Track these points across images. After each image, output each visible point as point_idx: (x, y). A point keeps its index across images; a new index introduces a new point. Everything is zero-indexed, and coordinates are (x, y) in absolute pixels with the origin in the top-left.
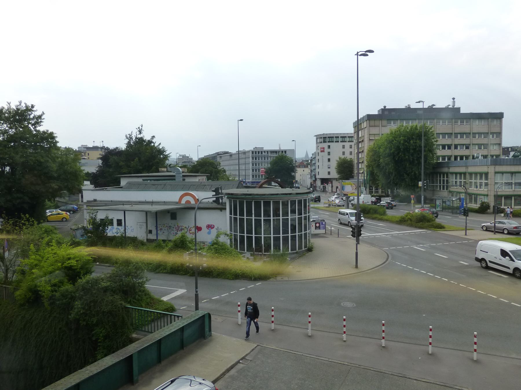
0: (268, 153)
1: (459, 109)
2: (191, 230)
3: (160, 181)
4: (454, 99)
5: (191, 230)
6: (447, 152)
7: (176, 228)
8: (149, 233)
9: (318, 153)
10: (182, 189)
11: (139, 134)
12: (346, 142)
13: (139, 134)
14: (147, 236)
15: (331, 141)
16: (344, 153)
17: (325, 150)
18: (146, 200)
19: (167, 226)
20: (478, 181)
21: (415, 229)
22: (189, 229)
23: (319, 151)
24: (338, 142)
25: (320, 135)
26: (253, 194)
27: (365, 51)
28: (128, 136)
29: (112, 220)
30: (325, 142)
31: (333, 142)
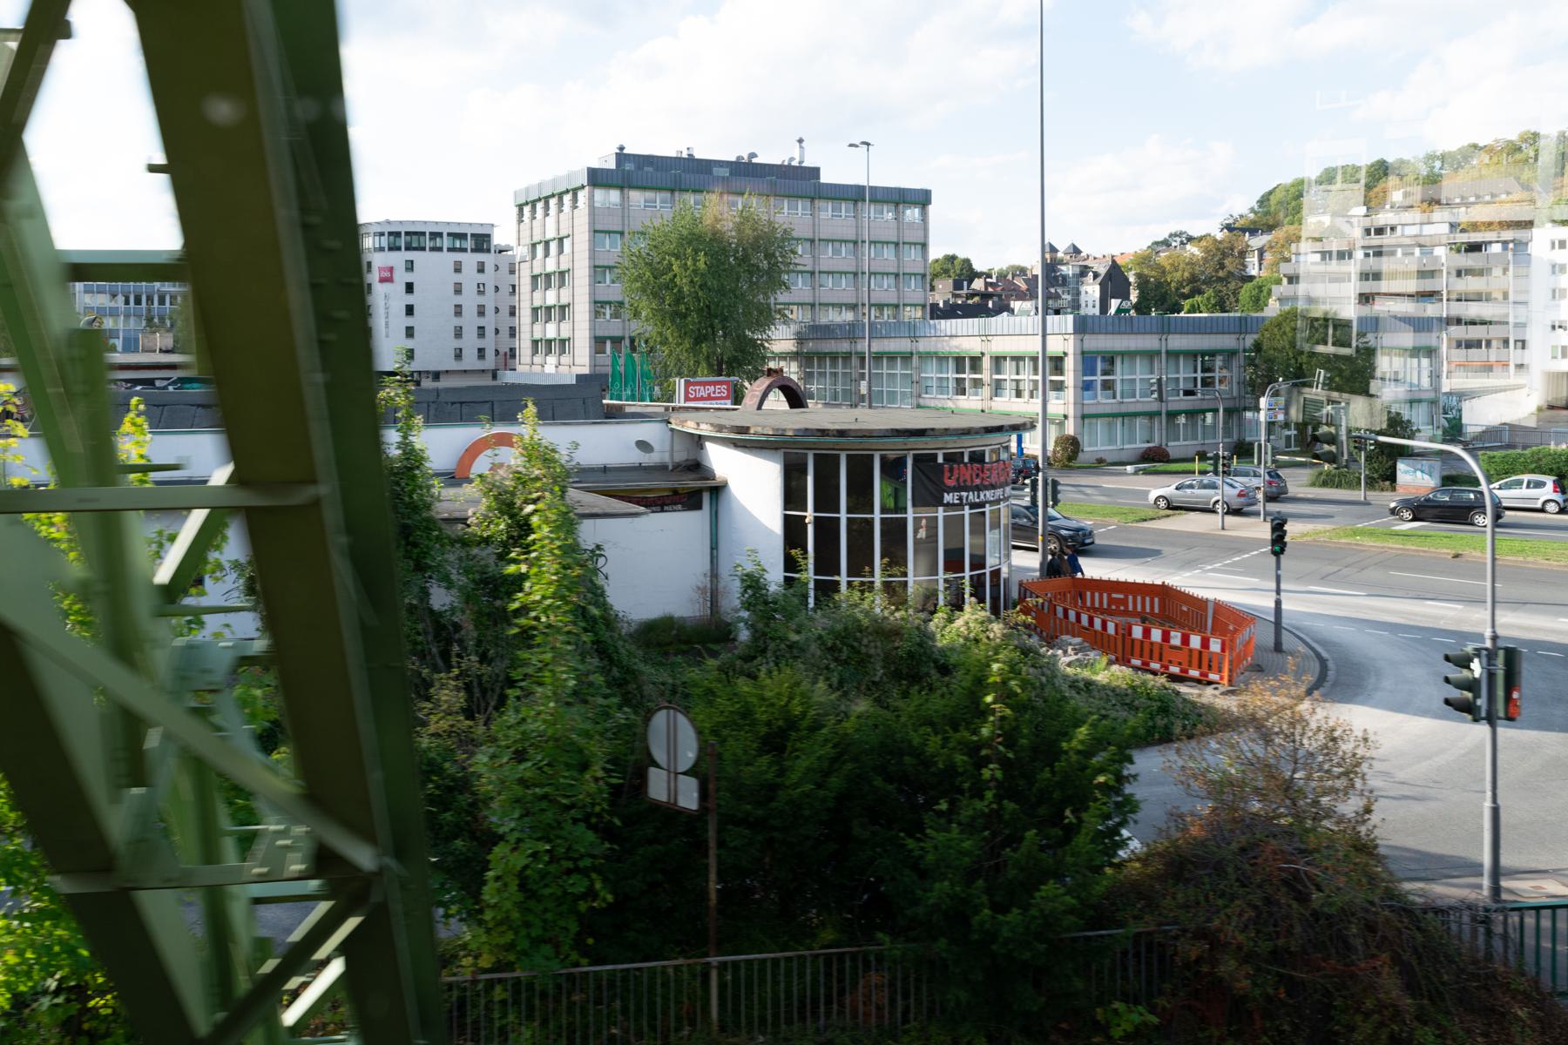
1: (815, 172)
4: (801, 141)
17: (396, 276)
24: (440, 249)
26: (933, 429)
30: (394, 248)
31: (423, 249)
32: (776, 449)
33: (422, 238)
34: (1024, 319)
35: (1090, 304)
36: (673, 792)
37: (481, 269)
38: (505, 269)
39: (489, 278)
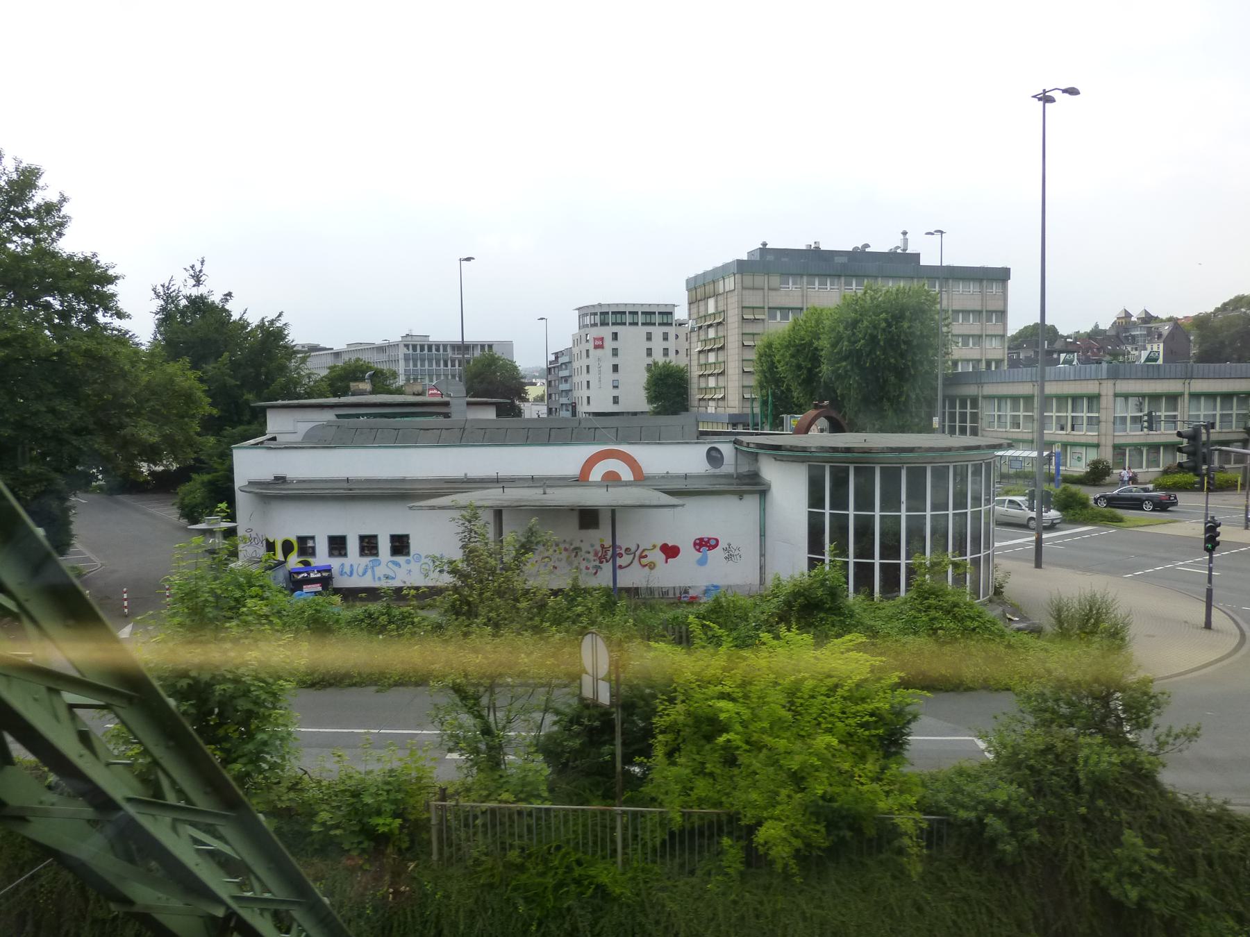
0: (445, 350)
1: (918, 255)
2: (646, 556)
3: (395, 417)
4: (905, 233)
5: (646, 556)
6: (972, 352)
7: (596, 554)
9: (588, 351)
10: (593, 440)
11: (194, 286)
12: (654, 324)
13: (194, 286)
15: (619, 321)
16: (649, 352)
18: (466, 475)
19: (566, 550)
21: (1070, 526)
22: (638, 554)
23: (591, 346)
24: (637, 324)
25: (593, 306)
26: (920, 448)
27: (1063, 88)
28: (160, 290)
30: (604, 324)
31: (625, 324)
32: (803, 462)
33: (653, 316)
36: (596, 692)
39: (671, 344)
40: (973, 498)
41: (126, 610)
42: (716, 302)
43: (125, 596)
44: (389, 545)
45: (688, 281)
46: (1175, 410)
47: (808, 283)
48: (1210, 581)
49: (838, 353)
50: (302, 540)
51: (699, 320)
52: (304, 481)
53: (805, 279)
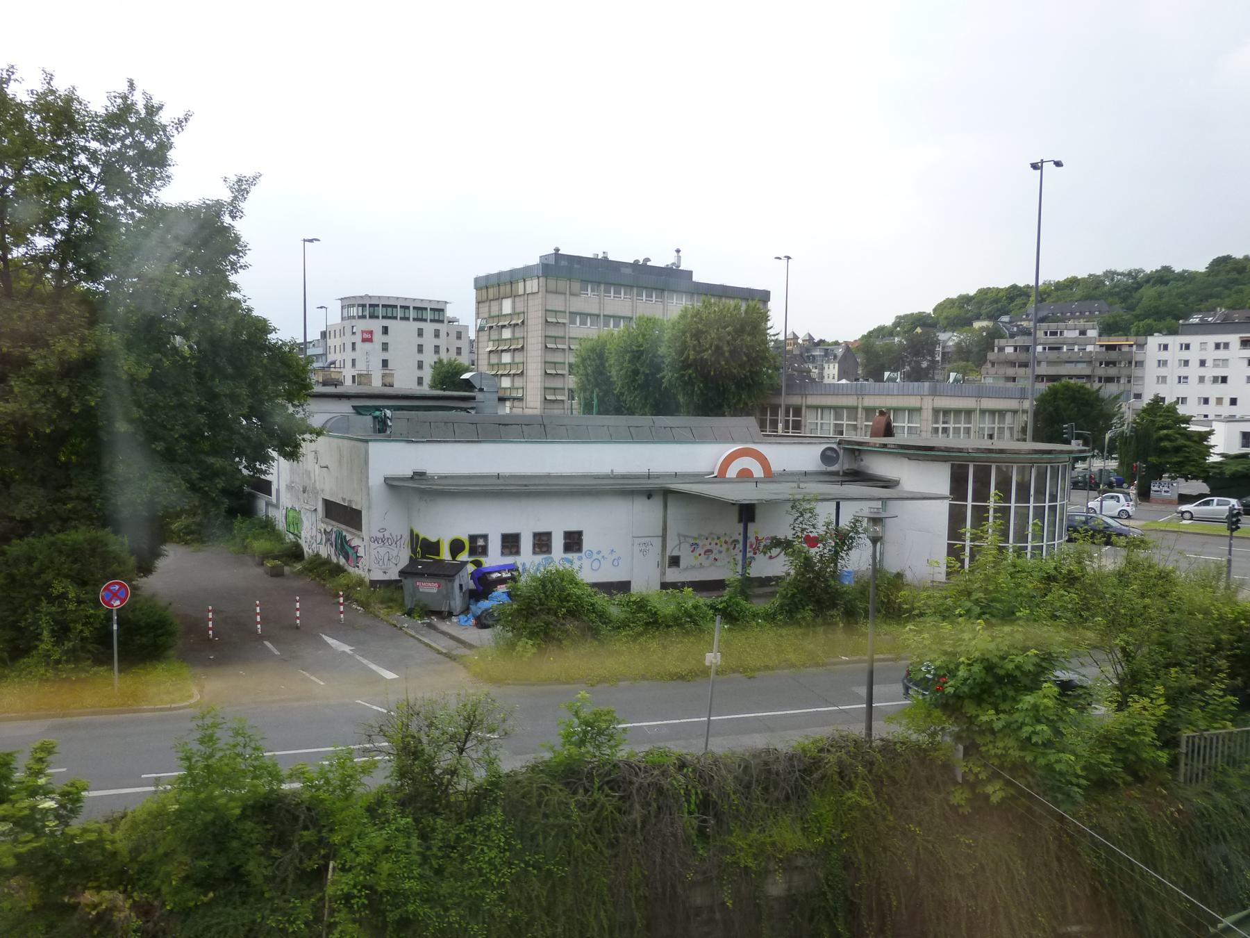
1: (690, 273)
4: (678, 251)
8: (670, 566)
9: (354, 344)
10: (733, 441)
14: (663, 574)
19: (726, 542)
20: (962, 425)
23: (358, 338)
24: (408, 319)
25: (362, 297)
29: (438, 543)
30: (373, 316)
31: (395, 318)
34: (891, 384)
35: (831, 377)
37: (437, 334)
38: (453, 335)
39: (442, 342)
40: (1036, 492)
41: (298, 621)
42: (514, 303)
43: (342, 608)
44: (563, 542)
45: (477, 280)
46: (970, 423)
47: (605, 292)
48: (1230, 554)
49: (683, 362)
50: (473, 539)
51: (491, 320)
52: (446, 477)
53: (635, 290)
